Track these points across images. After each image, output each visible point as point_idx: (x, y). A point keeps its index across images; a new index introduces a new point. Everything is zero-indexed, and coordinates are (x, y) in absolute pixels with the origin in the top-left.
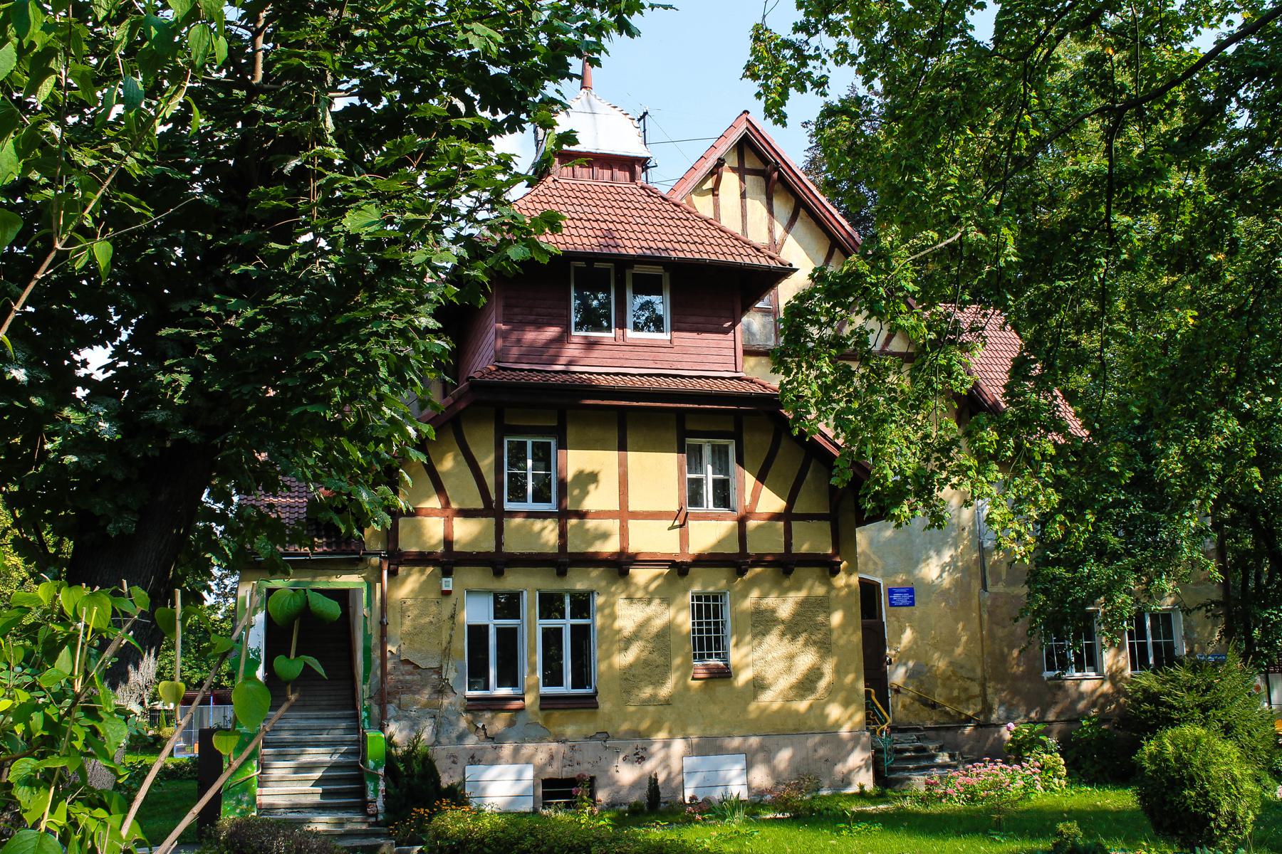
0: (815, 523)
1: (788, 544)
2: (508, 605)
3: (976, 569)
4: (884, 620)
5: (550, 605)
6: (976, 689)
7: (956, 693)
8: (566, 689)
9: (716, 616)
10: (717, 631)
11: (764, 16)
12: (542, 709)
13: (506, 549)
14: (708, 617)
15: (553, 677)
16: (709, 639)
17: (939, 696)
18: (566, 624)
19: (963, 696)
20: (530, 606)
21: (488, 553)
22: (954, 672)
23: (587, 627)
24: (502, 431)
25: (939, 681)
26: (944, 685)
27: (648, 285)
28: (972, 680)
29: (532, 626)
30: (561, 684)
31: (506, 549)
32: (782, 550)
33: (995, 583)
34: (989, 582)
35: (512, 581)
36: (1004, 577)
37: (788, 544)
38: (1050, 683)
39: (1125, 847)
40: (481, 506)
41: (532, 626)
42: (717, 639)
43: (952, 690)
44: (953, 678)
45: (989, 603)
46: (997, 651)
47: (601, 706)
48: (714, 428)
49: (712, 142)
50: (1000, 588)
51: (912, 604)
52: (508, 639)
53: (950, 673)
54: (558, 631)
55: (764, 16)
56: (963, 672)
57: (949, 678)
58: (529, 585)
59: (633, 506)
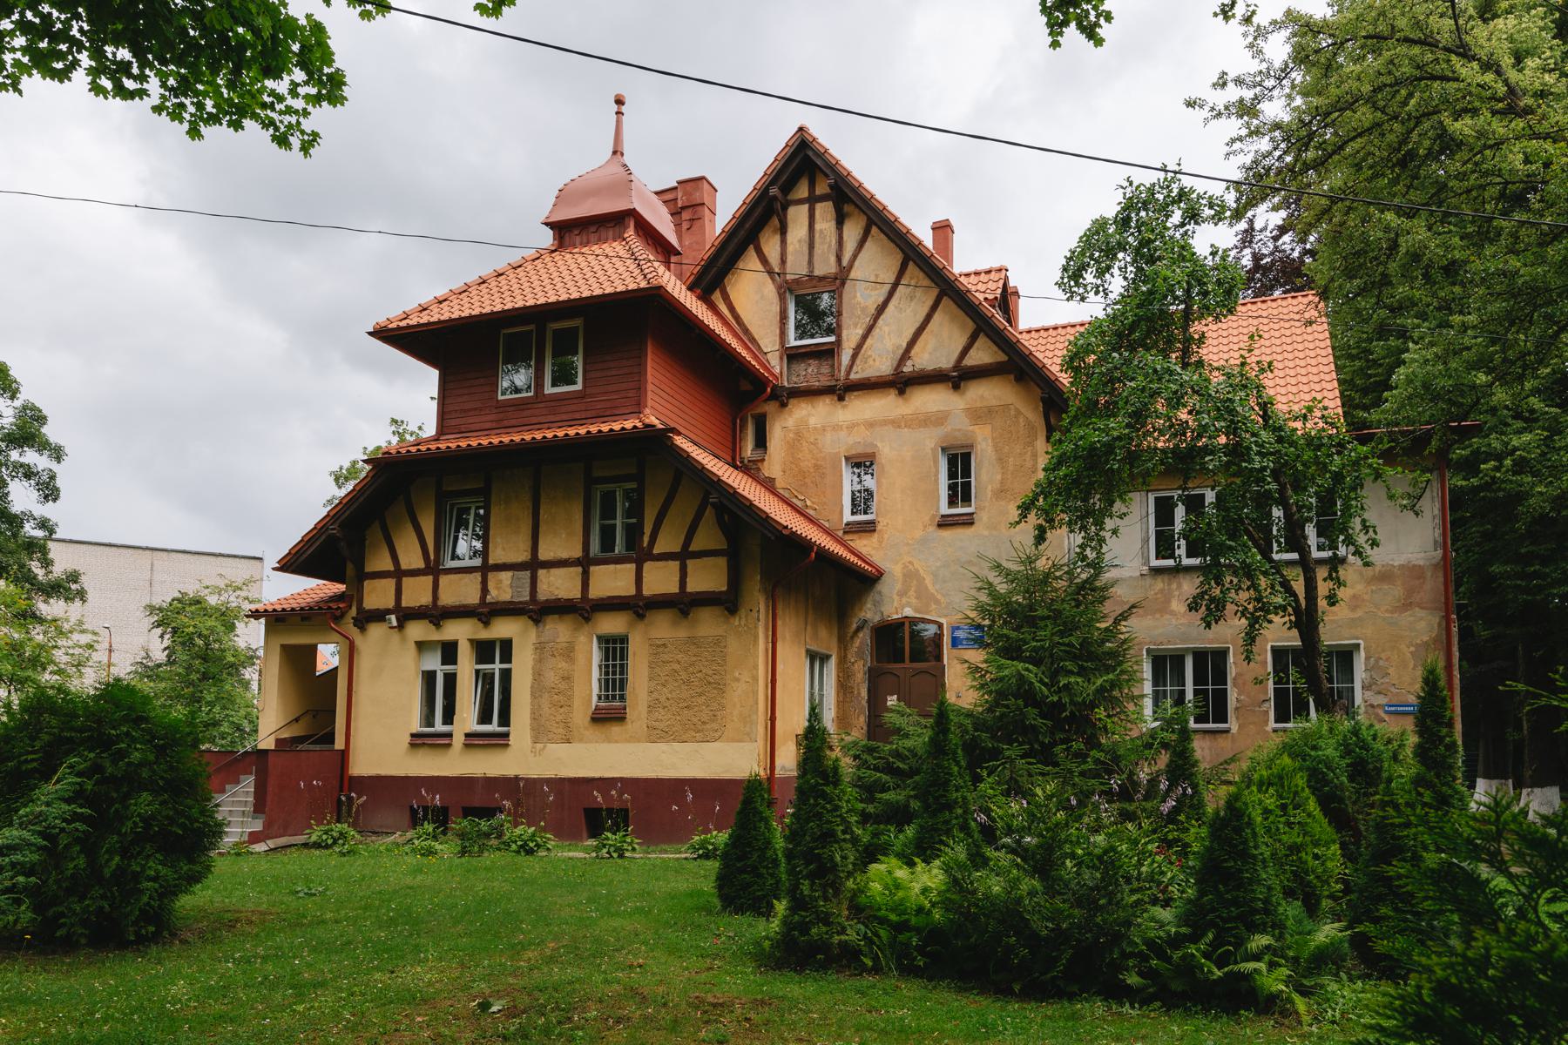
4: (945, 662)
5: (484, 650)
8: (493, 727)
9: (622, 659)
10: (622, 673)
14: (614, 659)
15: (485, 717)
18: (497, 666)
41: (466, 667)
42: (622, 681)
52: (451, 680)
58: (460, 632)
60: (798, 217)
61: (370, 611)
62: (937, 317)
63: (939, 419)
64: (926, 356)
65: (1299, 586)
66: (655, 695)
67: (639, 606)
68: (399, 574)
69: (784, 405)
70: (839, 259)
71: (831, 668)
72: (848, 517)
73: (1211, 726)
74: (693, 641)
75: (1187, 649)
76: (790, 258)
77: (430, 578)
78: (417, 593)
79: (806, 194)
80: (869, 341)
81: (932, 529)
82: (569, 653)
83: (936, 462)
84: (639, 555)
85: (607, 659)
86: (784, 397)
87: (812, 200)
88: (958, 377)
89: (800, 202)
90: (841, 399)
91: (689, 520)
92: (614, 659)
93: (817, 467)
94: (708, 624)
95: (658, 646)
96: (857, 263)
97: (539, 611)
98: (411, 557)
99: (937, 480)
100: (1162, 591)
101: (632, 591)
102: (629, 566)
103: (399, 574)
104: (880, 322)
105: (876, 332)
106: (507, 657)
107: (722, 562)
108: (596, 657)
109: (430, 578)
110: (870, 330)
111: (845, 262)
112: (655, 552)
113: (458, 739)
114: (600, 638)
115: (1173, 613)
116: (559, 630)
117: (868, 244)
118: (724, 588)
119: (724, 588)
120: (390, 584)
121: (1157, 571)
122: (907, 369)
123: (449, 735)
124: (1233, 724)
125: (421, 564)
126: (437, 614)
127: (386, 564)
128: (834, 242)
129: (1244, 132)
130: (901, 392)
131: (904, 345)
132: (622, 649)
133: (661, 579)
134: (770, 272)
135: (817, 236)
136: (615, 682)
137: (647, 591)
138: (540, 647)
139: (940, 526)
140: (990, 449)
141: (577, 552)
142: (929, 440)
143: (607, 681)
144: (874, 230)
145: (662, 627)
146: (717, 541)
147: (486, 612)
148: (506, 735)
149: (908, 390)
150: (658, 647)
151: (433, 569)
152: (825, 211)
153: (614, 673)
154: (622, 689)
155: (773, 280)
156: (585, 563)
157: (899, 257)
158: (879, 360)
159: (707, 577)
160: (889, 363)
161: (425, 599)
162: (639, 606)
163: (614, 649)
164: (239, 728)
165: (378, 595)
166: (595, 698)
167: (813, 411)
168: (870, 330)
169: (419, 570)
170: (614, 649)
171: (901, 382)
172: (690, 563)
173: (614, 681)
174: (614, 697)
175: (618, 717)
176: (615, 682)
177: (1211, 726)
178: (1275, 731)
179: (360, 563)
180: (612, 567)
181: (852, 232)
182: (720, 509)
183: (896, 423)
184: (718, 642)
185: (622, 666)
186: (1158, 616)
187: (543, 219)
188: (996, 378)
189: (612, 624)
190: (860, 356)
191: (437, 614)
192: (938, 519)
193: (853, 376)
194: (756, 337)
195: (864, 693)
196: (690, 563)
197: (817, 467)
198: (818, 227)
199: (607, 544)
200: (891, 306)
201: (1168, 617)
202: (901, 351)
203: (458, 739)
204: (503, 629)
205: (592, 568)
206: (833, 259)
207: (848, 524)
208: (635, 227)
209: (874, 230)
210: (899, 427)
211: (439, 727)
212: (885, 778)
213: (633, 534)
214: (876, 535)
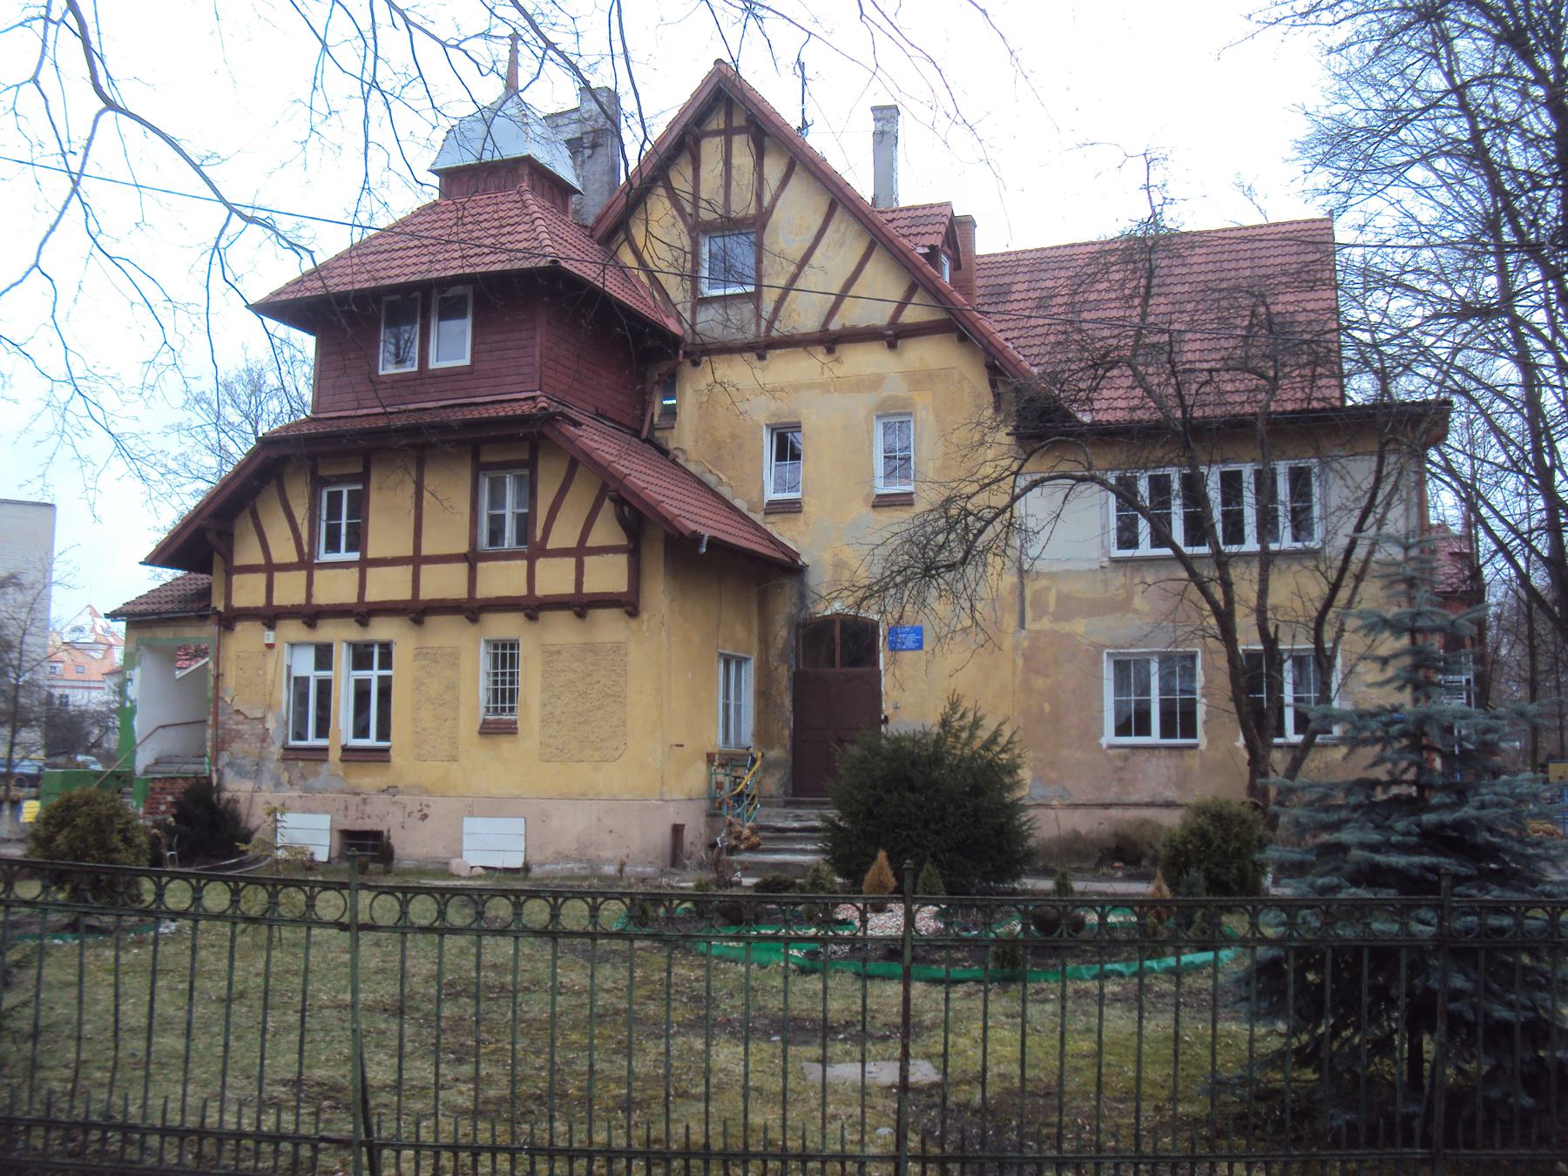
0: (611, 557)
1: (579, 582)
2: (324, 657)
4: (882, 667)
5: (361, 657)
8: (371, 741)
9: (512, 666)
10: (512, 683)
11: (325, 47)
12: (342, 760)
13: (276, 602)
14: (504, 667)
15: (361, 731)
16: (503, 691)
18: (374, 675)
20: (342, 656)
21: (348, 605)
23: (390, 678)
24: (318, 483)
27: (451, 311)
29: (344, 678)
31: (276, 602)
32: (464, 595)
33: (1038, 617)
34: (1029, 615)
35: (329, 632)
36: (1052, 608)
37: (579, 582)
38: (1111, 752)
40: (588, 544)
41: (344, 678)
42: (512, 691)
45: (1026, 644)
49: (1021, 78)
50: (1045, 624)
51: (920, 647)
52: (325, 688)
55: (325, 47)
58: (340, 635)
59: (426, 550)
60: (711, 150)
61: (240, 609)
62: (870, 267)
63: (876, 382)
65: (1218, 594)
66: (549, 708)
67: (532, 607)
68: (270, 568)
69: (696, 364)
70: (759, 197)
71: (749, 674)
72: (771, 495)
73: (1178, 741)
74: (590, 648)
75: (1153, 653)
77: (303, 574)
78: (289, 590)
79: (722, 126)
81: (866, 510)
82: (453, 659)
83: (870, 432)
84: (533, 550)
85: (496, 667)
86: (703, 351)
87: (728, 133)
88: (894, 336)
89: (716, 133)
90: (761, 357)
91: (586, 512)
92: (504, 667)
94: (608, 627)
95: (552, 653)
96: (779, 204)
97: (417, 612)
98: (284, 550)
99: (871, 453)
100: (1124, 586)
103: (270, 568)
106: (386, 662)
107: (622, 560)
108: (484, 663)
109: (303, 574)
112: (549, 546)
113: (335, 755)
114: (488, 642)
115: (1136, 612)
116: (446, 633)
117: (792, 182)
118: (625, 589)
119: (625, 589)
120: (260, 579)
121: (1117, 561)
122: (835, 325)
123: (325, 749)
124: (1201, 739)
125: (295, 559)
126: (312, 615)
127: (257, 558)
132: (512, 655)
133: (555, 578)
134: (681, 211)
135: (734, 172)
136: (504, 694)
137: (540, 591)
138: (421, 653)
139: (874, 506)
140: (931, 419)
141: (463, 547)
142: (861, 405)
143: (496, 691)
145: (561, 630)
146: (619, 538)
147: (363, 613)
150: (551, 655)
151: (306, 564)
152: (741, 145)
153: (503, 682)
154: (512, 700)
155: (684, 220)
156: (472, 558)
157: (822, 205)
158: (804, 315)
159: (608, 575)
161: (298, 598)
162: (532, 607)
163: (505, 655)
165: (248, 591)
166: (482, 711)
170: (505, 655)
171: (830, 341)
173: (503, 691)
174: (503, 709)
175: (510, 729)
176: (504, 694)
177: (1178, 741)
178: (1111, 747)
179: (228, 557)
180: (502, 563)
181: (774, 169)
182: (620, 502)
183: (824, 388)
184: (618, 649)
185: (512, 674)
186: (1119, 615)
187: (428, 166)
188: (936, 337)
189: (504, 626)
191: (312, 615)
192: (872, 499)
193: (774, 333)
195: (787, 701)
197: (734, 437)
199: (496, 535)
201: (1130, 616)
203: (335, 755)
204: (382, 630)
207: (771, 503)
208: (530, 174)
210: (828, 391)
211: (312, 741)
212: (1448, 863)
213: (525, 524)
214: (802, 516)
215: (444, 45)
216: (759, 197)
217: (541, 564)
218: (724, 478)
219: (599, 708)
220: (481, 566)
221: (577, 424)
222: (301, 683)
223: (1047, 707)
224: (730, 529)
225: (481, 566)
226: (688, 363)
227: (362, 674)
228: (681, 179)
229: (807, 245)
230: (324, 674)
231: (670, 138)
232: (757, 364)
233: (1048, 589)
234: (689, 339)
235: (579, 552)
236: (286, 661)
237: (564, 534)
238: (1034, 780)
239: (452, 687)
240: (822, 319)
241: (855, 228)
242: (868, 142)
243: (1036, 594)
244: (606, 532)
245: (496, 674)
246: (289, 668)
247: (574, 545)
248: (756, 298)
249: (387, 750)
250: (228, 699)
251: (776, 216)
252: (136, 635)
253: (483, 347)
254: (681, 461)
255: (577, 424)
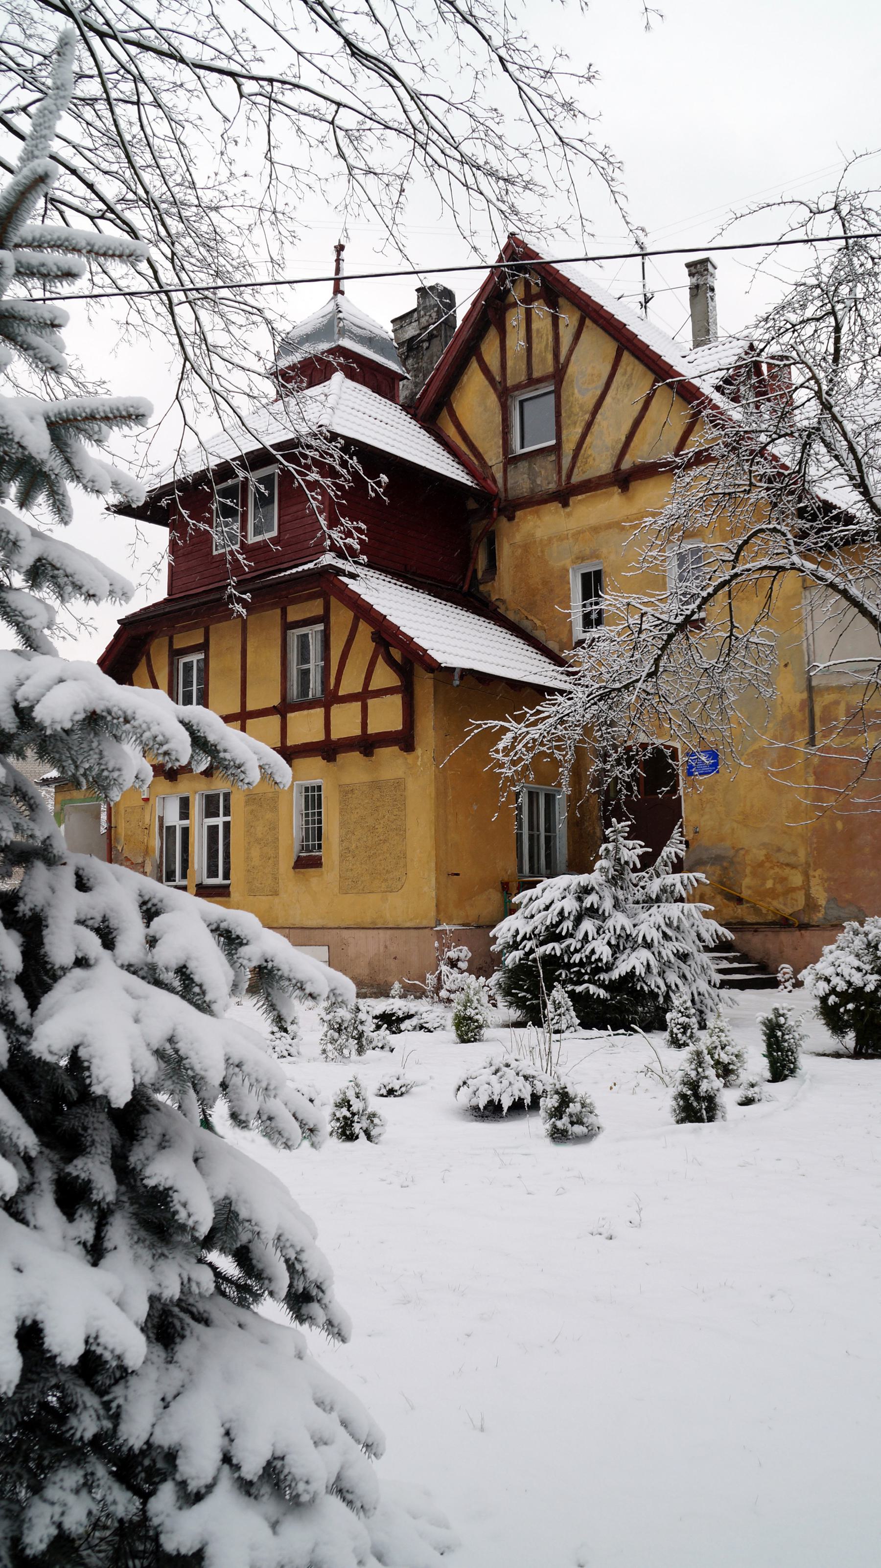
3: (801, 717)
6: (797, 879)
7: (769, 884)
8: (219, 880)
13: (334, 736)
17: (747, 886)
18: (219, 821)
19: (779, 888)
20: (197, 807)
22: (768, 857)
23: (181, 818)
25: (748, 870)
26: (754, 874)
28: (793, 866)
30: (217, 876)
33: (826, 734)
39: (238, 1000)
41: (199, 824)
43: (764, 880)
44: (767, 865)
46: (827, 827)
47: (232, 894)
48: (308, 615)
52: (186, 831)
53: (762, 858)
54: (217, 827)
56: (783, 858)
57: (761, 865)
59: (251, 707)
60: (515, 319)
64: (646, 448)
69: (511, 518)
70: (556, 355)
76: (510, 363)
80: (588, 439)
85: (307, 808)
90: (565, 504)
93: (545, 583)
96: (573, 358)
101: (321, 737)
102: (318, 710)
104: (598, 417)
105: (595, 428)
110: (589, 426)
111: (562, 359)
117: (584, 336)
118: (400, 727)
119: (400, 727)
122: (626, 465)
128: (550, 339)
129: (862, 196)
130: (565, 504)
131: (623, 438)
135: (534, 334)
144: (588, 322)
148: (228, 886)
149: (633, 485)
152: (540, 310)
160: (609, 461)
164: (439, 987)
167: (539, 522)
168: (589, 426)
169: (404, 703)
172: (371, 702)
175: (316, 863)
190: (580, 457)
194: (481, 450)
196: (371, 702)
197: (545, 583)
198: (535, 326)
200: (608, 399)
202: (620, 446)
205: (289, 715)
206: (550, 357)
209: (588, 322)
215: (92, 218)
216: (556, 355)
217: (335, 709)
218: (538, 623)
219: (385, 841)
220: (290, 716)
221: (353, 576)
222: (171, 830)
223: (839, 825)
224: (507, 663)
225: (290, 716)
226: (504, 520)
227: (212, 821)
228: (490, 350)
229: (599, 392)
230: (185, 823)
231: (475, 314)
232: (562, 512)
233: (837, 703)
234: (502, 495)
235: (363, 696)
236: (158, 813)
237: (351, 684)
238: (828, 902)
239: (273, 827)
240: (615, 461)
241: (640, 368)
242: (685, 295)
243: (826, 708)
244: (384, 677)
245: (307, 815)
246: (161, 819)
247: (359, 689)
248: (557, 449)
249: (228, 886)
250: (120, 848)
251: (570, 370)
252: (61, 797)
253: (286, 518)
254: (501, 611)
255: (353, 576)
